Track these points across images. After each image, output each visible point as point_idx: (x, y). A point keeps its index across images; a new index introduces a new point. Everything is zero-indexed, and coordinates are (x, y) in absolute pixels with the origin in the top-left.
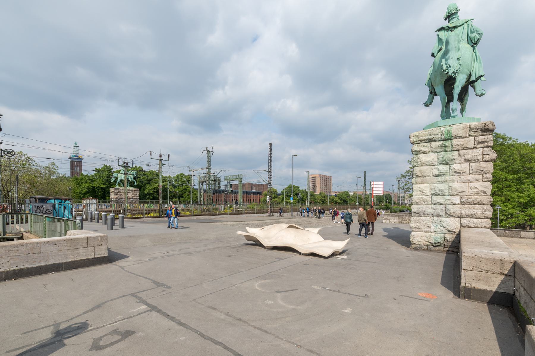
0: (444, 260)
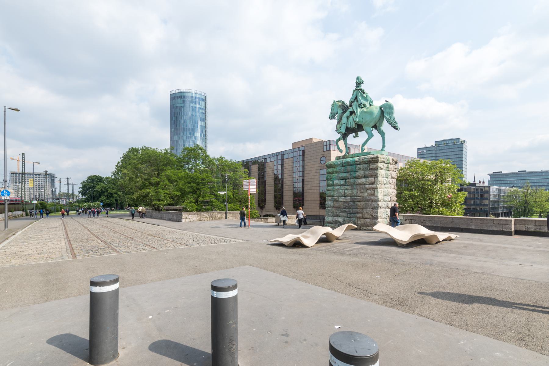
0: (184, 344)
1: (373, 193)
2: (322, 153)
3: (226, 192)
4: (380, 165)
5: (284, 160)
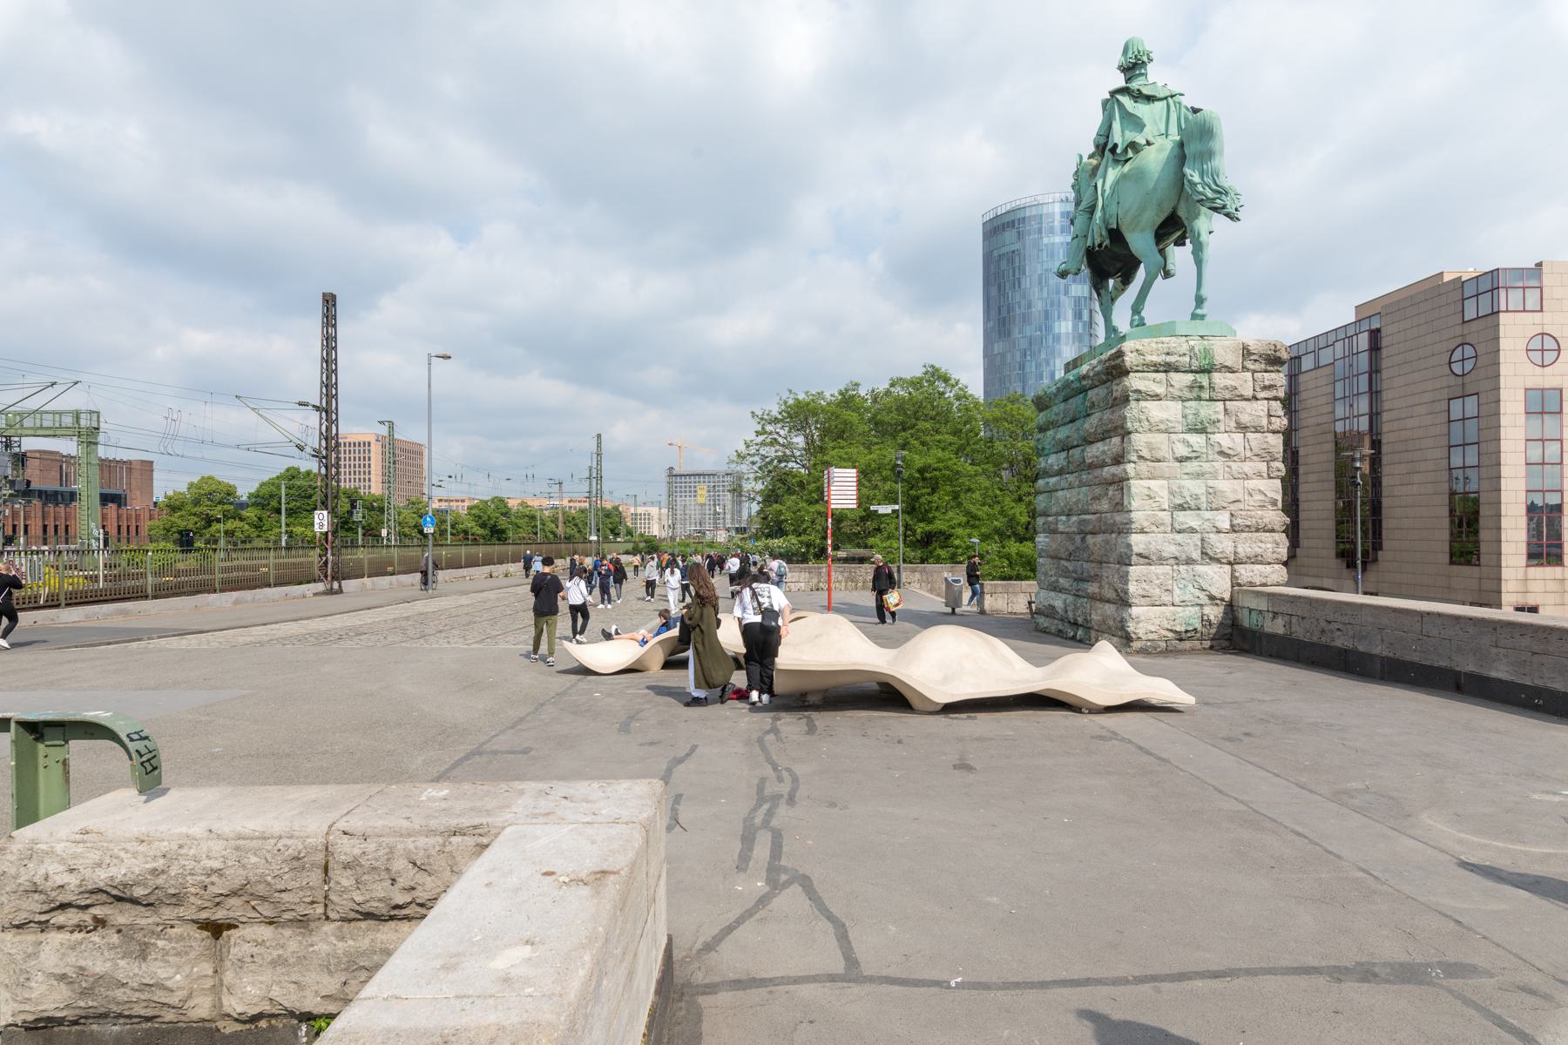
1: (1118, 500)
2: (1458, 330)
3: (897, 507)
4: (1135, 382)
5: (1302, 378)
